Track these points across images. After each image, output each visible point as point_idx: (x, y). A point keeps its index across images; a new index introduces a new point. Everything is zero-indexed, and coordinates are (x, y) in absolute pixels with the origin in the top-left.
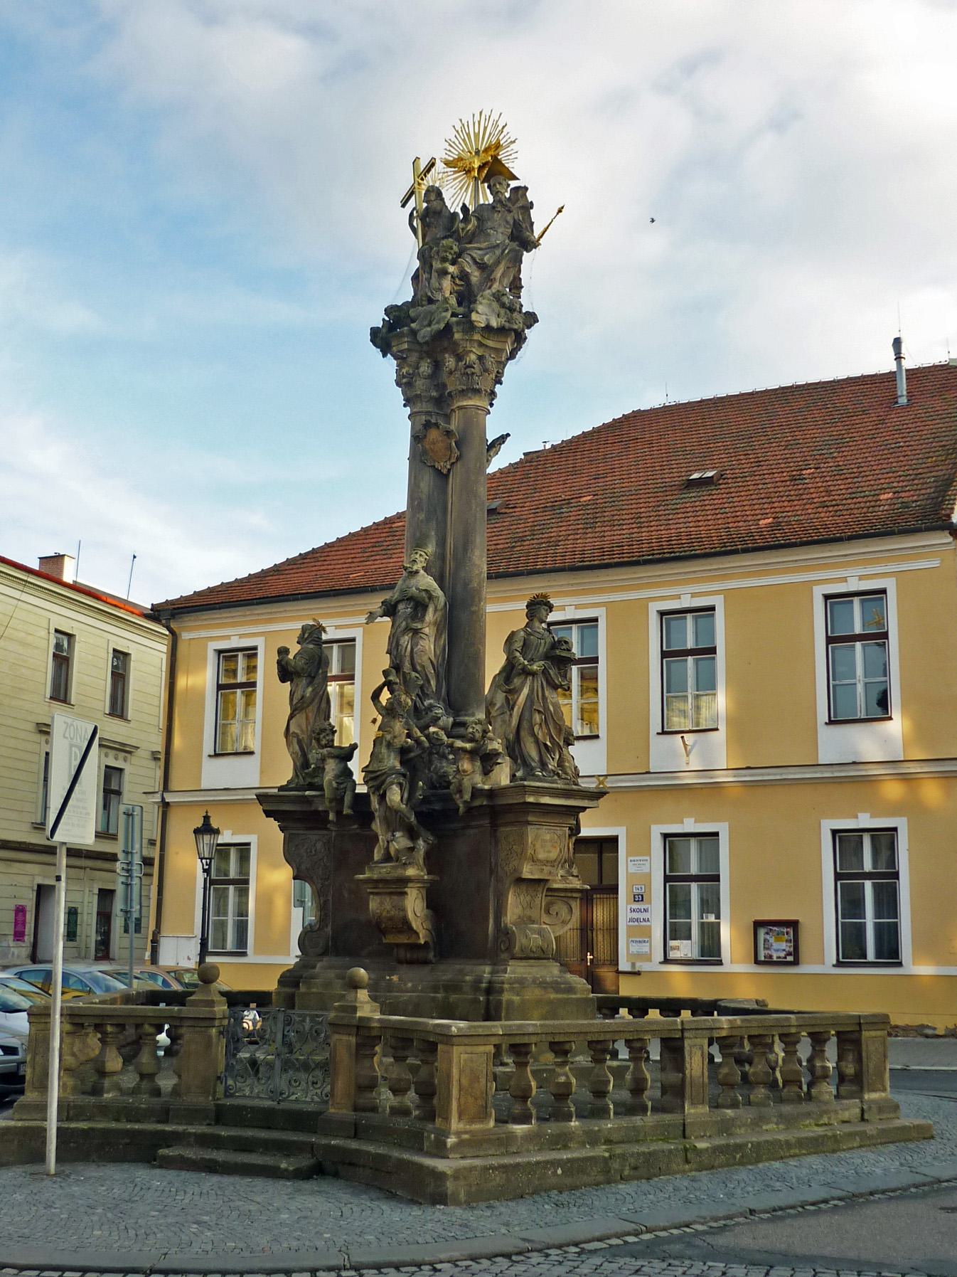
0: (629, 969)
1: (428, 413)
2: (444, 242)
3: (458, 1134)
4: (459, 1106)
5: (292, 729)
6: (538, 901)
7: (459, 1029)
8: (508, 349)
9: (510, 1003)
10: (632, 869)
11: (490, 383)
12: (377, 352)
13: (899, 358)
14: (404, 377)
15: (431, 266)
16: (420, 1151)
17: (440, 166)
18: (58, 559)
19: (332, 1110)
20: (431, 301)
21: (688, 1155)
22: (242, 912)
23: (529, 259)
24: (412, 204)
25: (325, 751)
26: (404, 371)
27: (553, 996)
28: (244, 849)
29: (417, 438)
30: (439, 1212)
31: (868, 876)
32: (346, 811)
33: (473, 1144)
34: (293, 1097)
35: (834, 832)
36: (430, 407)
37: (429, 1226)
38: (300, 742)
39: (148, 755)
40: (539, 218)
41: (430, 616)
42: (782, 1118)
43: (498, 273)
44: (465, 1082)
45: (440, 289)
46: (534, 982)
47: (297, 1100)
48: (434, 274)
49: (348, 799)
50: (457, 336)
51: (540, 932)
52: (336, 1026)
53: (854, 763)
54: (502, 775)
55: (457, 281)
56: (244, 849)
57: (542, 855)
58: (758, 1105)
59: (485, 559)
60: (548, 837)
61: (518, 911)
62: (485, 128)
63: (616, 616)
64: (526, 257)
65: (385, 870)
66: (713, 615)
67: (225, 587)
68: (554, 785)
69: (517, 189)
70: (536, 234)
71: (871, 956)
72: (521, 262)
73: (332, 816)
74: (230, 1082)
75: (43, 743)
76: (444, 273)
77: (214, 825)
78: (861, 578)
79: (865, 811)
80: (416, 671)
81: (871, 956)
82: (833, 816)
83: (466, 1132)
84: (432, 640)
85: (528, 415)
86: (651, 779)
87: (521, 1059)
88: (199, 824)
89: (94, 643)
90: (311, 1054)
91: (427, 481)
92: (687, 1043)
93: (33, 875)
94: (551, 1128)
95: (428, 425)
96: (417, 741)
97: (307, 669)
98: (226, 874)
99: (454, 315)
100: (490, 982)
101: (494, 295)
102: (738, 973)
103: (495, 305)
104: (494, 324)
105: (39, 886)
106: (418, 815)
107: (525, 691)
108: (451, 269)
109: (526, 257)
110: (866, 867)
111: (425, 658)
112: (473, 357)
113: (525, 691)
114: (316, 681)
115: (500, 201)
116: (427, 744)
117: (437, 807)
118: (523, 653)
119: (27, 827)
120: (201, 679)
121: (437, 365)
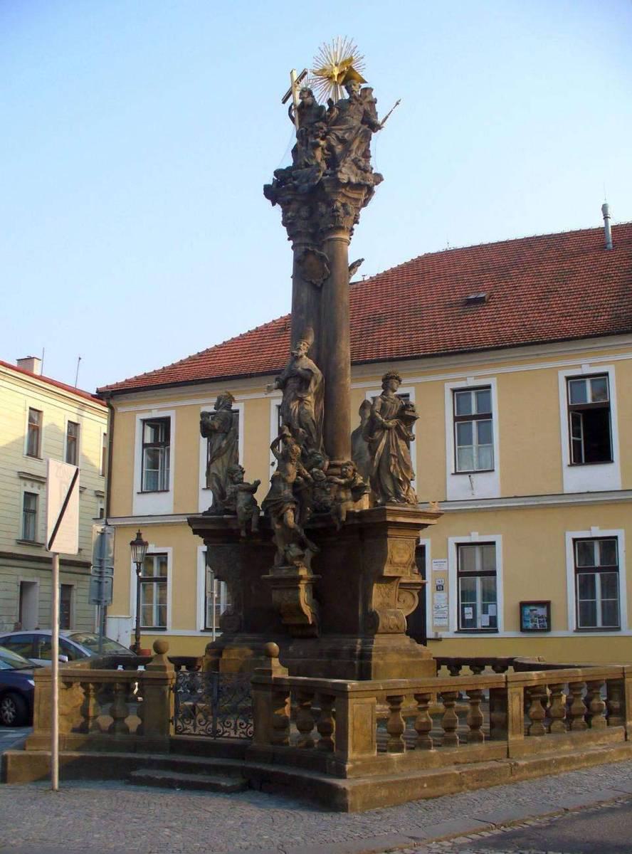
0: (433, 637)
1: (306, 244)
2: (317, 124)
3: (353, 761)
4: (353, 741)
5: (213, 470)
6: (393, 591)
7: (353, 686)
8: (363, 198)
9: (377, 665)
10: (436, 568)
11: (351, 222)
12: (269, 202)
13: (606, 217)
14: (289, 219)
15: (307, 141)
16: (324, 772)
17: (310, 75)
18: (30, 359)
19: (255, 744)
20: (307, 165)
21: (514, 768)
22: (162, 600)
23: (377, 139)
24: (290, 101)
25: (237, 486)
26: (289, 214)
27: (406, 659)
28: (163, 557)
29: (298, 262)
30: (340, 818)
31: (598, 570)
32: (254, 529)
33: (366, 767)
34: (226, 735)
35: (575, 540)
36: (308, 240)
37: (339, 828)
38: (218, 480)
39: (92, 493)
40: (381, 110)
41: (312, 388)
42: (574, 742)
43: (354, 147)
44: (357, 724)
45: (314, 157)
46: (393, 650)
47: (228, 737)
48: (310, 147)
49: (254, 520)
50: (327, 189)
51: (396, 615)
52: (257, 685)
53: (588, 492)
54: (365, 503)
55: (326, 151)
56: (163, 557)
57: (397, 559)
58: (556, 732)
59: (349, 347)
60: (401, 546)
61: (380, 600)
62: (342, 49)
63: (432, 393)
64: (373, 135)
65: (284, 572)
66: (489, 392)
67: (147, 376)
68: (406, 509)
69: (366, 89)
70: (380, 120)
71: (599, 624)
72: (370, 139)
73: (243, 534)
74: (179, 723)
75: (23, 486)
76: (316, 146)
77: (144, 538)
78: (591, 365)
79: (596, 526)
80: (302, 427)
81: (599, 624)
82: (456, 534)
83: (358, 760)
84: (313, 405)
85: (379, 243)
86: (449, 506)
87: (395, 707)
88: (134, 538)
89: (57, 415)
90: (238, 703)
91: (306, 293)
92: (509, 691)
93: (18, 576)
94: (419, 754)
95: (306, 252)
96: (306, 479)
97: (220, 429)
98: (151, 574)
99: (325, 174)
100: (362, 651)
101: (353, 160)
102: (507, 639)
103: (354, 168)
104: (353, 180)
105: (22, 583)
106: (307, 531)
107: (384, 441)
108: (322, 143)
109: (373, 135)
110: (596, 562)
111: (309, 418)
112: (339, 204)
113: (384, 441)
114: (229, 436)
115: (355, 97)
116: (312, 480)
117: (319, 525)
118: (382, 413)
119: (14, 543)
120: (136, 437)
121: (312, 211)
